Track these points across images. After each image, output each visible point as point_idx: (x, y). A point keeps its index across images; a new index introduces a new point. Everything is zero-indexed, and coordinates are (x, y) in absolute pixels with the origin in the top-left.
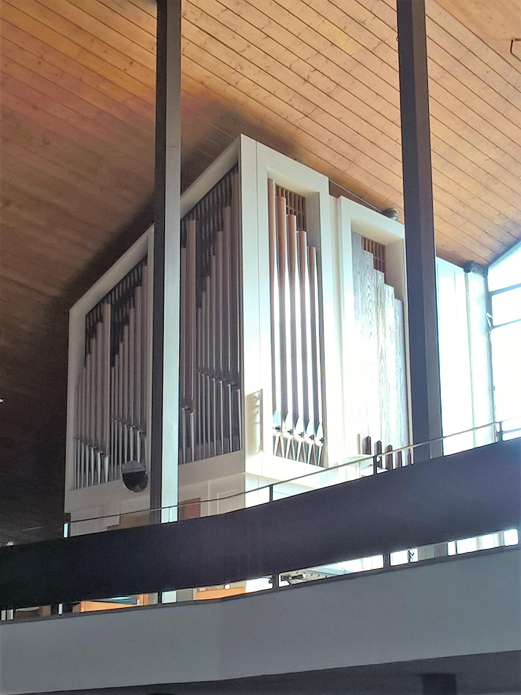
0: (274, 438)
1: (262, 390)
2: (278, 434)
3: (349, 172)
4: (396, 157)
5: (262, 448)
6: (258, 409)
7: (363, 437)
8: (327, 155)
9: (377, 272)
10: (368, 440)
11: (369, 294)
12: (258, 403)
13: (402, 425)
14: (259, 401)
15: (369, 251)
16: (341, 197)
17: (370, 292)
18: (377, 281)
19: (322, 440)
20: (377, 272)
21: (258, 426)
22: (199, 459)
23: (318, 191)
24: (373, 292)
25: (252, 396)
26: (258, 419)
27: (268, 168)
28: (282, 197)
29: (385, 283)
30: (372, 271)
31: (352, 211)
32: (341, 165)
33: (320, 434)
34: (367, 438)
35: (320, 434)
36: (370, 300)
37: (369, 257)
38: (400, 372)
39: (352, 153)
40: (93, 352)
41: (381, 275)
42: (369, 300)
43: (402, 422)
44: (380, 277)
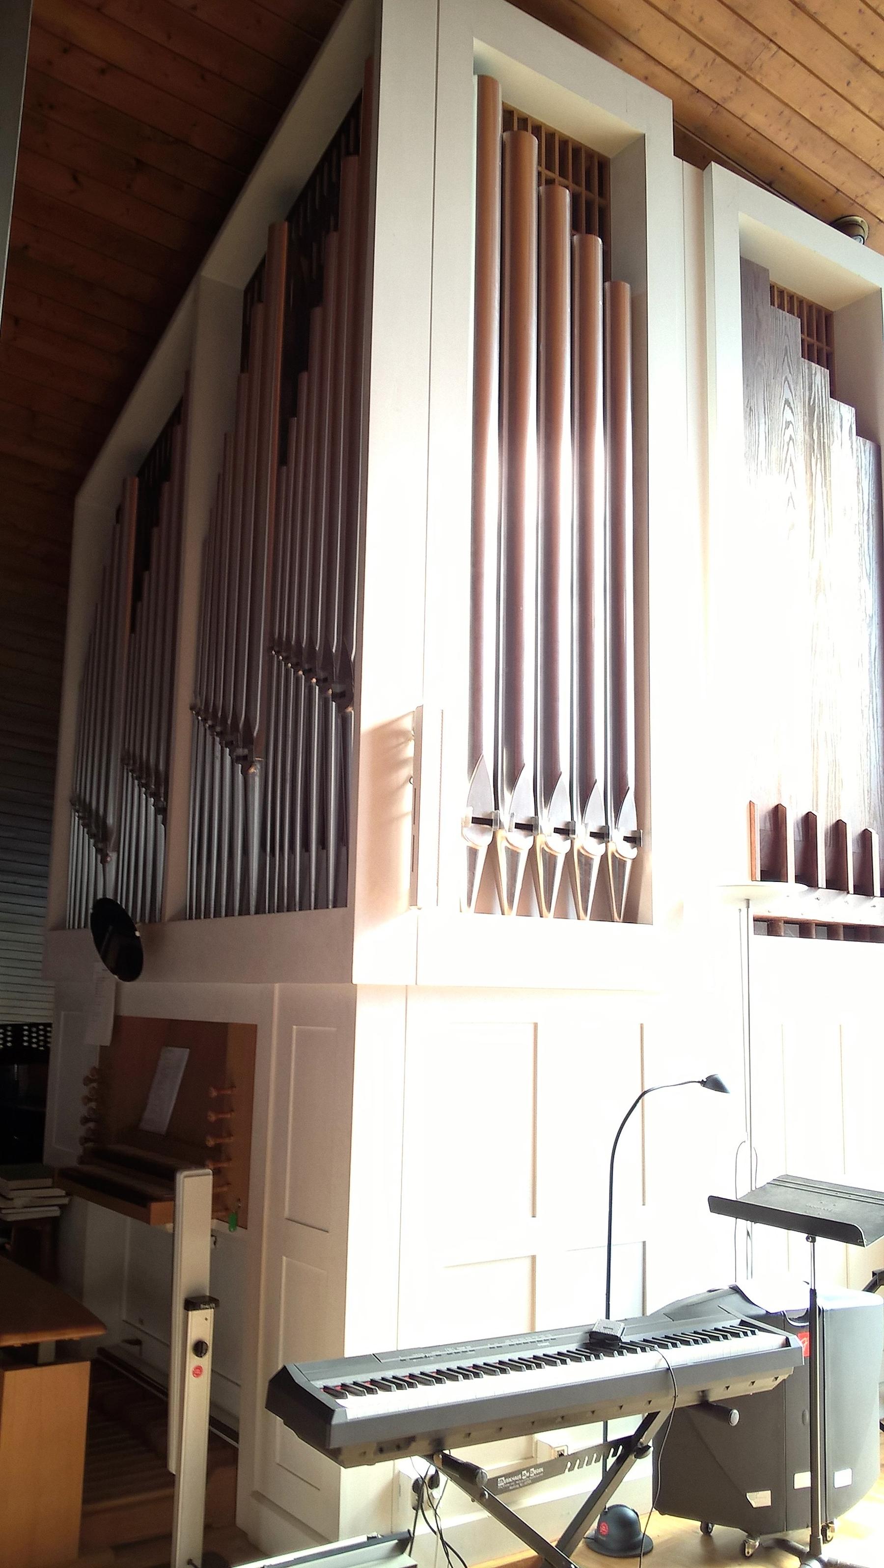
0: (473, 853)
1: (420, 708)
2: (482, 841)
3: (737, 106)
4: (862, 52)
5: (413, 900)
6: (407, 771)
7: (765, 806)
8: (672, 51)
9: (810, 368)
10: (777, 815)
11: (788, 423)
12: (409, 751)
13: (874, 762)
14: (412, 744)
15: (791, 311)
16: (715, 167)
17: (796, 417)
18: (810, 389)
19: (634, 840)
20: (810, 368)
21: (406, 825)
22: (249, 914)
23: (641, 130)
24: (800, 417)
25: (389, 735)
26: (406, 803)
27: (480, 46)
28: (524, 133)
29: (832, 395)
30: (798, 363)
31: (747, 212)
32: (715, 83)
33: (628, 822)
34: (777, 807)
35: (628, 822)
36: (791, 438)
37: (790, 328)
38: (870, 626)
39: (740, 43)
40: (154, 566)
41: (820, 376)
42: (787, 439)
43: (873, 759)
44: (797, 323)
